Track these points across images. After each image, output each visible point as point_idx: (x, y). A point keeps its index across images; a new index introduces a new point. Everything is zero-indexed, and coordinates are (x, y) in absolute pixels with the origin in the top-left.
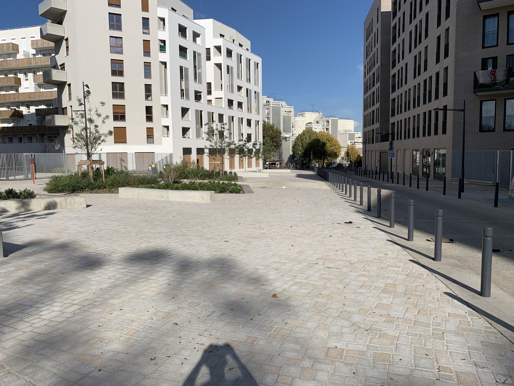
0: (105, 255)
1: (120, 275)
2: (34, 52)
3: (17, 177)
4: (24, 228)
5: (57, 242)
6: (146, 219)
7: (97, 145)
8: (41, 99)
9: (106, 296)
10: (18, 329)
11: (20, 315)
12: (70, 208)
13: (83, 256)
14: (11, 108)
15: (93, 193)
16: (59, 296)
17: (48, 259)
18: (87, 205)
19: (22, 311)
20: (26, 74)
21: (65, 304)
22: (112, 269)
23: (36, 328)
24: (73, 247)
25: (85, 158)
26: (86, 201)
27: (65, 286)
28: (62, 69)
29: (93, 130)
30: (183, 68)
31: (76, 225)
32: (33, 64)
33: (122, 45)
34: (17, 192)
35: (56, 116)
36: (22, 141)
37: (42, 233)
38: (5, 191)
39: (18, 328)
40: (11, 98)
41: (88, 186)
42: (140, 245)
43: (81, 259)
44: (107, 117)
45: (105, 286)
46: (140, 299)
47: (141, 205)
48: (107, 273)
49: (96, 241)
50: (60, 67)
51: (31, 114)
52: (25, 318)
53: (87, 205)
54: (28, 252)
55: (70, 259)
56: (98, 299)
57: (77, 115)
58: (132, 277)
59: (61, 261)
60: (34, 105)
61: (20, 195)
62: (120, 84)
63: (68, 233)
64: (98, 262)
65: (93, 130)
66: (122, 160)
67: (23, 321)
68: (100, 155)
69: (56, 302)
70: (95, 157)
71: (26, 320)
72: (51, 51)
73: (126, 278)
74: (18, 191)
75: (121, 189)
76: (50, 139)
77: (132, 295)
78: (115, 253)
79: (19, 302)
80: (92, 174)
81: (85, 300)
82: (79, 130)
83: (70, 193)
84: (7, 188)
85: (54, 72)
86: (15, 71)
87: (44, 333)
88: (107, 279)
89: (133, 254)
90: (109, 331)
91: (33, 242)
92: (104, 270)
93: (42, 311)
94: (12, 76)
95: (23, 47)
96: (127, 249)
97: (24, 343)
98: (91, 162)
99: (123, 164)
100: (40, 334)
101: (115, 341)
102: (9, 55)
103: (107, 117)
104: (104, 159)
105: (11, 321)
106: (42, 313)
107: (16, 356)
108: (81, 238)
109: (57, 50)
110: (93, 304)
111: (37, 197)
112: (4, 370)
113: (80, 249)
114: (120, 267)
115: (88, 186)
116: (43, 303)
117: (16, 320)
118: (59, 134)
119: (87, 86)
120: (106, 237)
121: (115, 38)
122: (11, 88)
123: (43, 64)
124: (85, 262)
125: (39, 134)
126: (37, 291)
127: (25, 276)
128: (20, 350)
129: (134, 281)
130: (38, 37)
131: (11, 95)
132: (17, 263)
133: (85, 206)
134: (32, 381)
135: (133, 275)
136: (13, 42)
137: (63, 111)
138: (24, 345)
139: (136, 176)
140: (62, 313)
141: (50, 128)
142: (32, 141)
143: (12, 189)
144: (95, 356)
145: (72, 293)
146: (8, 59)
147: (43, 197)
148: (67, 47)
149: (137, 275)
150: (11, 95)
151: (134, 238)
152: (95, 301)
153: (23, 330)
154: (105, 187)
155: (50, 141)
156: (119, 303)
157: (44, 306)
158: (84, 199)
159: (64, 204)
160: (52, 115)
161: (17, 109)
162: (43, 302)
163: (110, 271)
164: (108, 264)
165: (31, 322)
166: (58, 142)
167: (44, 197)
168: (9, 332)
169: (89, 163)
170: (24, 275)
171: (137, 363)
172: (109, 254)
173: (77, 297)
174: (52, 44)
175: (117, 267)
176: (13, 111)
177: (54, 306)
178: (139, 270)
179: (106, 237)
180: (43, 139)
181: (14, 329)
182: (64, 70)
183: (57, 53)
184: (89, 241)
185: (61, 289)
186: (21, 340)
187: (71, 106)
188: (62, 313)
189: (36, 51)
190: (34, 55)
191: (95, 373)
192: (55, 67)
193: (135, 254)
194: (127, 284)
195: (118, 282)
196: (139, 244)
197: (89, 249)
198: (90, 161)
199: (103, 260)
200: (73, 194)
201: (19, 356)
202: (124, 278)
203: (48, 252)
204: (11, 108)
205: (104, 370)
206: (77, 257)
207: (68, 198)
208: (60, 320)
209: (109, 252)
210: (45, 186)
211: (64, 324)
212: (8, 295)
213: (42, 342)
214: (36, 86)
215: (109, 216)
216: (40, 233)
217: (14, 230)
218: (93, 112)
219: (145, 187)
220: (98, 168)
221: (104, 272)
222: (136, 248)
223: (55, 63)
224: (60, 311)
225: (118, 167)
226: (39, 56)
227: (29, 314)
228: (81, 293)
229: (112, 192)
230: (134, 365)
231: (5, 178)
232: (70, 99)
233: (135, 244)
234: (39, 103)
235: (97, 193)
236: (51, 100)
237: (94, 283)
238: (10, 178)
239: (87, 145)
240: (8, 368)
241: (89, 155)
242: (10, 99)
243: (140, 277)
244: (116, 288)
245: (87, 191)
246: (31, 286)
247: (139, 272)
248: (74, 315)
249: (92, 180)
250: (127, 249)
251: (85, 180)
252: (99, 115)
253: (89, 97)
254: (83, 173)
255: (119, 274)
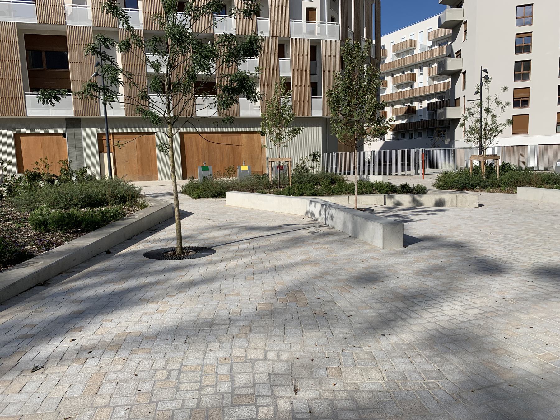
0: (505, 262)
1: (525, 288)
2: (430, 43)
3: (408, 172)
4: (418, 222)
5: (451, 240)
6: (554, 227)
7: (492, 137)
8: (434, 92)
9: (510, 307)
10: (423, 317)
11: (423, 305)
12: (461, 206)
13: (480, 258)
14: (406, 104)
15: (485, 192)
16: (459, 295)
17: (444, 255)
18: (479, 205)
19: (425, 301)
20: (421, 68)
21: (466, 305)
22: (515, 279)
23: (439, 321)
24: (468, 247)
25: (477, 152)
26: (478, 199)
27: (463, 287)
28: (457, 56)
29: (489, 121)
30: (44, 54)
31: (469, 224)
32: (429, 57)
33: (532, 13)
34: (410, 187)
35: (448, 108)
36: (413, 137)
37: (435, 229)
38: (401, 185)
39: (423, 316)
40: (407, 94)
41: (480, 183)
42: (549, 257)
43: (478, 262)
44: (507, 104)
45: (509, 296)
46: (556, 321)
47: (547, 210)
48: (510, 282)
49: (492, 245)
50: (455, 55)
51: (423, 109)
52: (428, 309)
53: (479, 205)
54: (424, 245)
55: (466, 260)
56: (502, 309)
57: (473, 105)
58: (542, 293)
59: (457, 260)
60: (427, 99)
61: (413, 190)
62: (524, 62)
63: (461, 232)
64: (497, 268)
65: (489, 121)
66: (520, 154)
67: (427, 311)
68: (494, 148)
69: (456, 300)
70: (488, 152)
71: (429, 310)
72: (447, 39)
73: (535, 293)
74: (411, 186)
75: (519, 189)
76: (440, 134)
77: (544, 315)
78: (517, 261)
79: (421, 292)
80: (484, 170)
81: (486, 306)
82: (474, 121)
83: (459, 190)
84: (402, 183)
85: (449, 61)
86: (411, 67)
87: (447, 327)
88: (510, 289)
89: (541, 266)
90: (518, 347)
91: (428, 237)
92: (506, 279)
93: (443, 306)
94: (409, 72)
95: (420, 41)
96: (532, 259)
97: (430, 332)
98: (484, 157)
99: (522, 159)
100: (443, 328)
101: (526, 360)
102: (407, 52)
103: (507, 104)
104: (498, 152)
105: (416, 308)
106: (444, 308)
107: (424, 341)
108: (476, 240)
109: (453, 37)
110: (495, 313)
111: (429, 192)
112: (415, 350)
113: (476, 251)
114: (525, 278)
115: (480, 183)
116: (443, 299)
117: (420, 308)
118: (449, 128)
119: (486, 71)
120: (505, 242)
121: (523, 7)
122: (407, 85)
123: (438, 55)
124: (484, 266)
125: (429, 129)
126: (436, 286)
127: (423, 268)
128: (427, 337)
129: (546, 299)
130: (436, 27)
131: (407, 92)
132: (416, 255)
133: (477, 206)
134: (440, 370)
135: (544, 291)
136: (412, 38)
137: (455, 102)
138: (430, 334)
139: (540, 174)
140: (463, 313)
141: (440, 121)
142: (422, 136)
143: (406, 184)
144: (504, 369)
145: (471, 295)
146: (406, 56)
147: (434, 193)
148: (465, 31)
149: (549, 292)
150: (407, 92)
151: (540, 248)
152: (498, 310)
153: (427, 319)
154: (499, 186)
155: (440, 135)
156: (528, 320)
157: (445, 302)
158: (476, 197)
159: (455, 201)
160: (444, 108)
161: (411, 105)
162: (443, 297)
163: (513, 280)
164: (509, 272)
165: (434, 313)
166: (447, 137)
167: (436, 193)
168: (416, 318)
169: (482, 158)
170: (423, 268)
171: (557, 394)
172: (510, 261)
173: (477, 301)
174: (449, 31)
175: (521, 278)
176: (407, 107)
177: (455, 304)
178: (551, 287)
179: (505, 242)
180: (433, 134)
181: (419, 316)
182: (460, 57)
183: (453, 40)
184: (485, 244)
185: (459, 288)
186: (427, 328)
187: (464, 96)
188: (463, 313)
189: (432, 42)
190: (430, 47)
191: (505, 386)
192: (451, 56)
193: (544, 268)
194: (536, 299)
195: (524, 296)
196: (548, 256)
197: (486, 253)
198: (483, 155)
199: (504, 267)
200: (462, 192)
201: (426, 342)
202: (531, 292)
203: (443, 249)
204: (406, 104)
205: (515, 387)
206: (474, 259)
207: (460, 195)
208: (462, 320)
209: (510, 259)
210: (434, 182)
211: (466, 325)
212: (411, 284)
213: (446, 337)
214: (430, 79)
215: (506, 219)
216: (433, 229)
217: (409, 223)
218: (492, 100)
219: (552, 188)
220: (491, 163)
221: (506, 281)
222: (544, 260)
223: (450, 52)
224: (461, 311)
225: (515, 162)
226: (436, 47)
227: (431, 306)
228: (482, 297)
229: (508, 192)
230: (552, 395)
231: (398, 173)
232: (464, 88)
233: (542, 255)
234: (431, 96)
235: (490, 191)
236: (444, 92)
237: (494, 290)
238: (402, 173)
239: (480, 138)
240: (418, 350)
241: (482, 149)
242: (405, 95)
243: (553, 295)
244: (522, 302)
245: (478, 189)
246: (430, 279)
247: (550, 289)
248: (476, 318)
249: (484, 178)
250: (532, 259)
251: (476, 178)
252: (499, 103)
253: (489, 84)
254: (473, 170)
255: (524, 287)
